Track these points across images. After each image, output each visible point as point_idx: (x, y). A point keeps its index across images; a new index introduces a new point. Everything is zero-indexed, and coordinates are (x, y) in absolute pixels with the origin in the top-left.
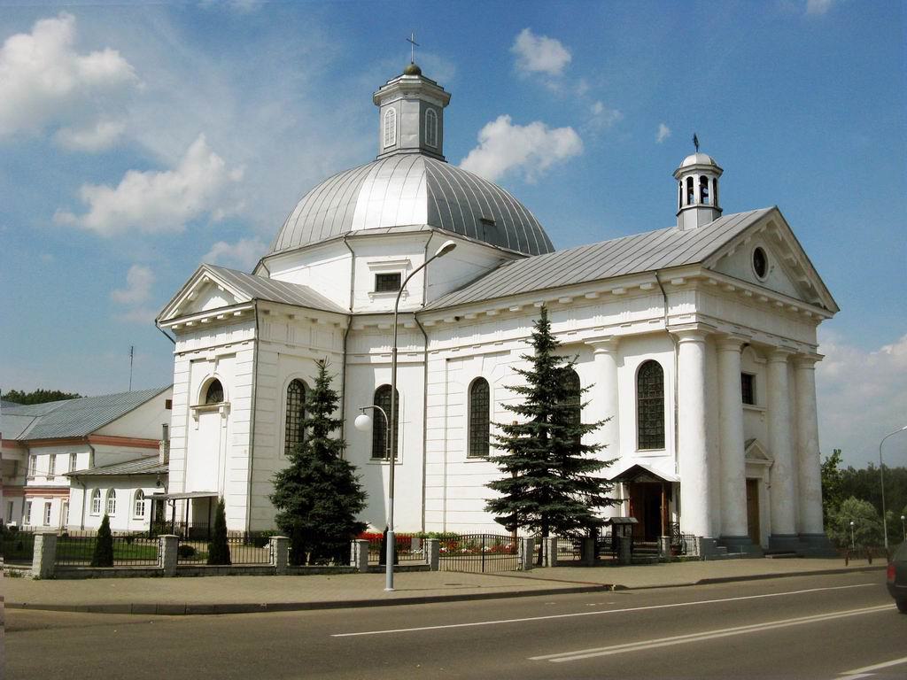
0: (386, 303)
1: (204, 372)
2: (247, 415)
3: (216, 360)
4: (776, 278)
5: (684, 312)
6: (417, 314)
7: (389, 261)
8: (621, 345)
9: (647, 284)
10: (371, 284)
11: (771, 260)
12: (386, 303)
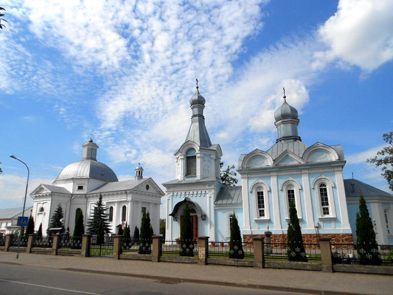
0: (81, 192)
1: (40, 206)
2: (49, 215)
3: (43, 203)
4: (151, 190)
5: (129, 198)
6: (85, 195)
7: (81, 183)
8: (120, 202)
9: (124, 192)
10: (77, 188)
11: (150, 186)
12: (81, 192)
